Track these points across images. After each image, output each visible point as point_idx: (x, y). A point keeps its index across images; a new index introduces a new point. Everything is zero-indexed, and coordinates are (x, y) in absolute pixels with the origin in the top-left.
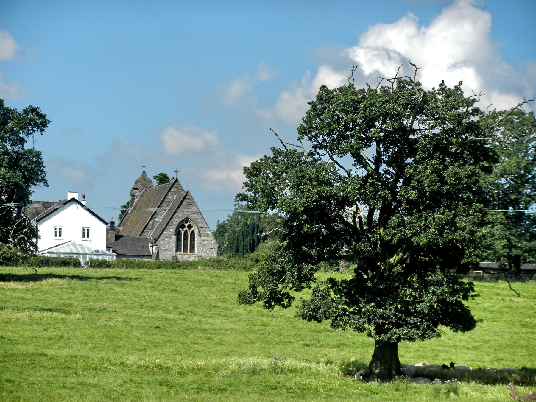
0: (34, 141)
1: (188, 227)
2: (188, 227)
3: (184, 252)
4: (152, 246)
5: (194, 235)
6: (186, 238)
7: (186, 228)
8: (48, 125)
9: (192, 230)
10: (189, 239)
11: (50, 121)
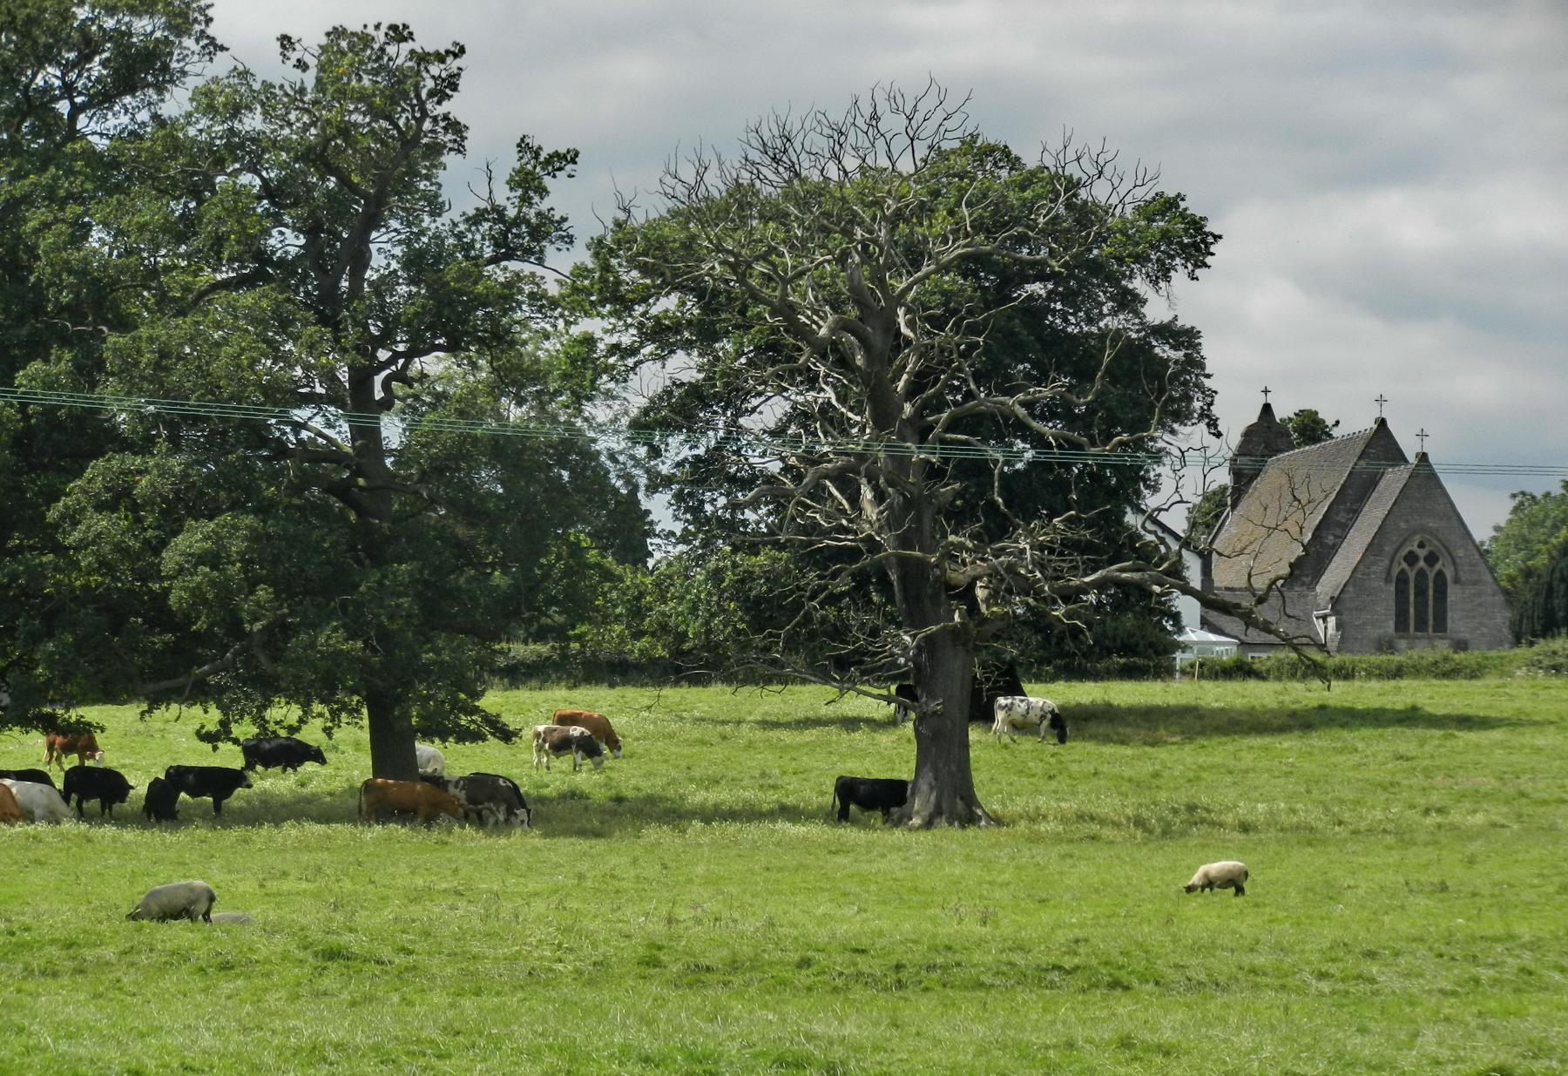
0: (1168, 300)
1: (1426, 559)
2: (1426, 559)
3: (1417, 629)
4: (1324, 618)
5: (1445, 583)
6: (1421, 592)
7: (1422, 564)
8: (1213, 249)
9: (1438, 566)
10: (1431, 592)
11: (1217, 237)
